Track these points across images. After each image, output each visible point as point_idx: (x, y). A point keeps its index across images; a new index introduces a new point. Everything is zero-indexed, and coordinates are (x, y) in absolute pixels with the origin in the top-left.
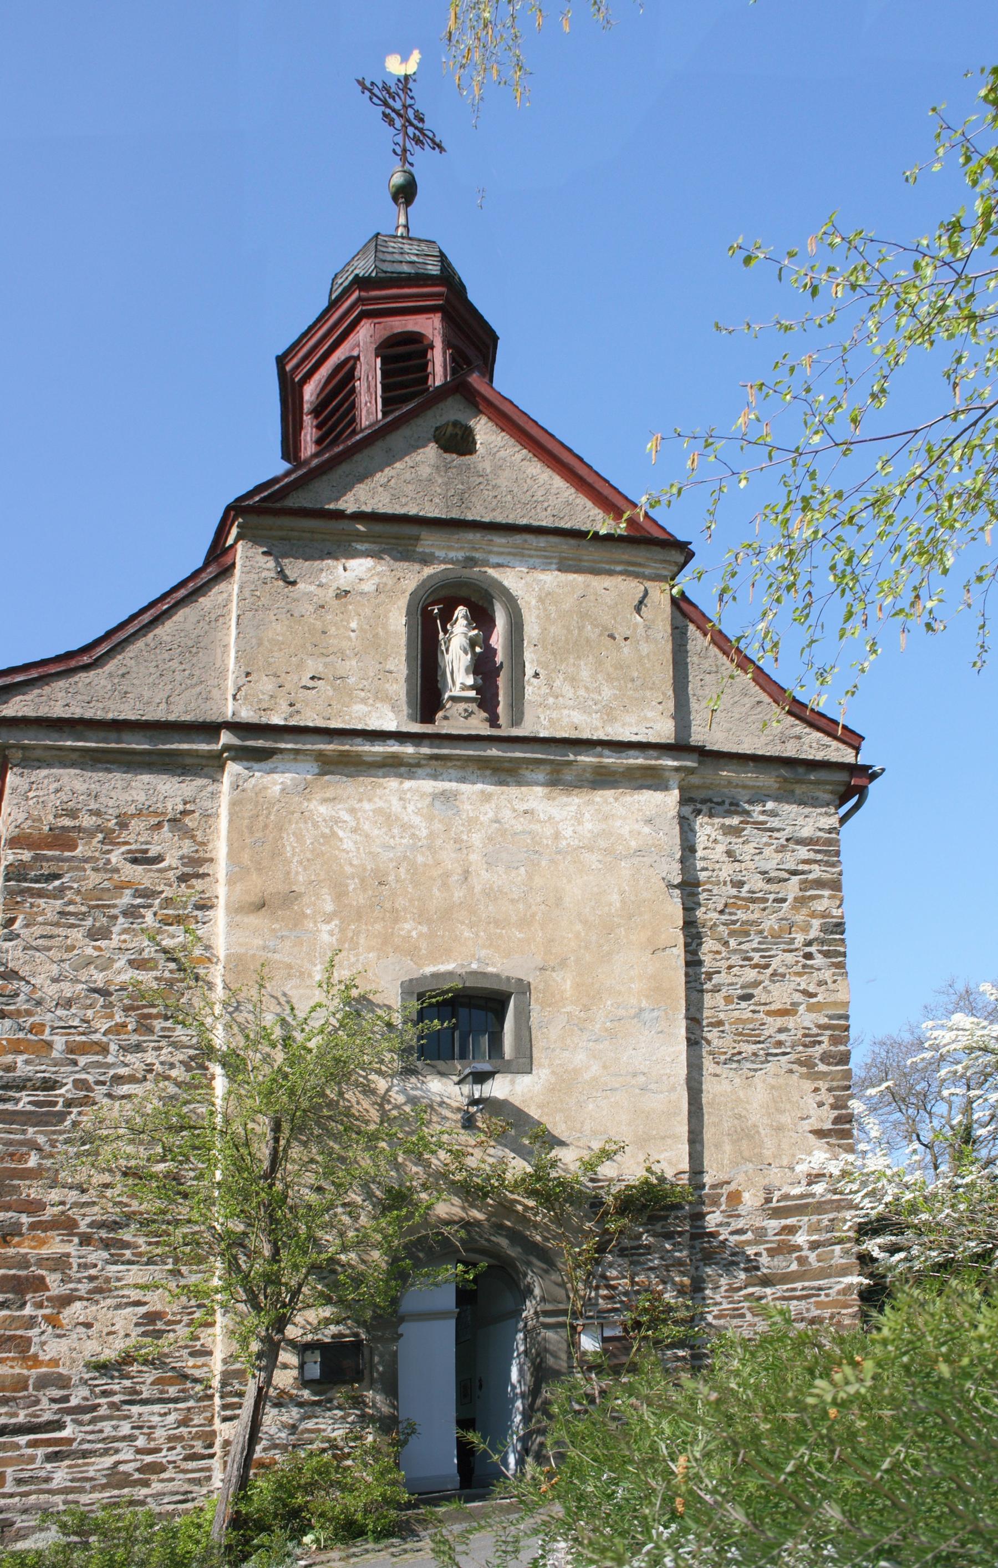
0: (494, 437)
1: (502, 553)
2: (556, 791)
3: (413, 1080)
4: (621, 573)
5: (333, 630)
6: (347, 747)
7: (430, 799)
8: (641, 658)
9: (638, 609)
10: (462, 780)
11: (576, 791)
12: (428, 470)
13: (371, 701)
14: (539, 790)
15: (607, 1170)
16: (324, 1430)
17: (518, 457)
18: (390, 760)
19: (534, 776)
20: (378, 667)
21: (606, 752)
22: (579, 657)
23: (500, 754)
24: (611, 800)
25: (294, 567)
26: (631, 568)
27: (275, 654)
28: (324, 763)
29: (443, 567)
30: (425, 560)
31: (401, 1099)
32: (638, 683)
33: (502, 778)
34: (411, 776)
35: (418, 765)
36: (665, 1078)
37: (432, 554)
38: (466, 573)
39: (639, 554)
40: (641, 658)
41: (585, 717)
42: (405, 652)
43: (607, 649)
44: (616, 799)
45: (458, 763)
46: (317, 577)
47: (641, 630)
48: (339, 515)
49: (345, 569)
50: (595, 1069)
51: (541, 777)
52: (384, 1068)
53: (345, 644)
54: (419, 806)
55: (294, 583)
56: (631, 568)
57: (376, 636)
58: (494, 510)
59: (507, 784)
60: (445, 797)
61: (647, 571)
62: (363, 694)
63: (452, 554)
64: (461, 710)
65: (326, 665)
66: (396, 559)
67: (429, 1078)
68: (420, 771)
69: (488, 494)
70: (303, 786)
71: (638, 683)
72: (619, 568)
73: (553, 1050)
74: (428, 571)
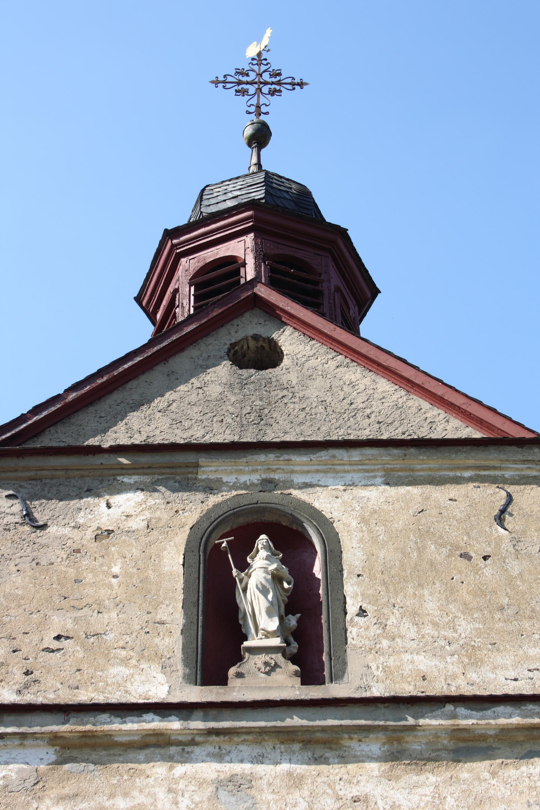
0: (301, 347)
1: (308, 472)
2: (400, 768)
4: (471, 479)
5: (89, 578)
6: (89, 727)
7: (212, 788)
8: (510, 581)
9: (500, 519)
10: (260, 759)
11: (430, 766)
12: (219, 389)
13: (134, 662)
14: (374, 768)
17: (332, 364)
18: (153, 740)
19: (364, 747)
20: (146, 617)
21: (461, 710)
22: (421, 585)
23: (305, 722)
24: (486, 775)
25: (43, 510)
26: (483, 473)
27: (12, 612)
28: (63, 747)
29: (234, 493)
30: (210, 488)
32: (510, 612)
33: (318, 753)
34: (185, 758)
35: (193, 743)
37: (219, 480)
38: (265, 497)
39: (492, 457)
40: (510, 581)
41: (435, 662)
42: (182, 597)
43: (460, 572)
44: (494, 774)
45: (250, 737)
46: (73, 518)
47: (507, 545)
48: (97, 450)
49: (109, 506)
51: (374, 746)
53: (103, 593)
54: (197, 799)
55: (44, 527)
56: (483, 473)
57: (145, 580)
58: (301, 423)
59: (326, 762)
60: (235, 784)
61: (508, 474)
62: (123, 653)
63: (243, 478)
64: (260, 664)
65: (76, 620)
66: (174, 490)
68: (197, 750)
69: (294, 407)
70: (33, 780)
71: (510, 612)
72: (467, 474)
74: (214, 500)
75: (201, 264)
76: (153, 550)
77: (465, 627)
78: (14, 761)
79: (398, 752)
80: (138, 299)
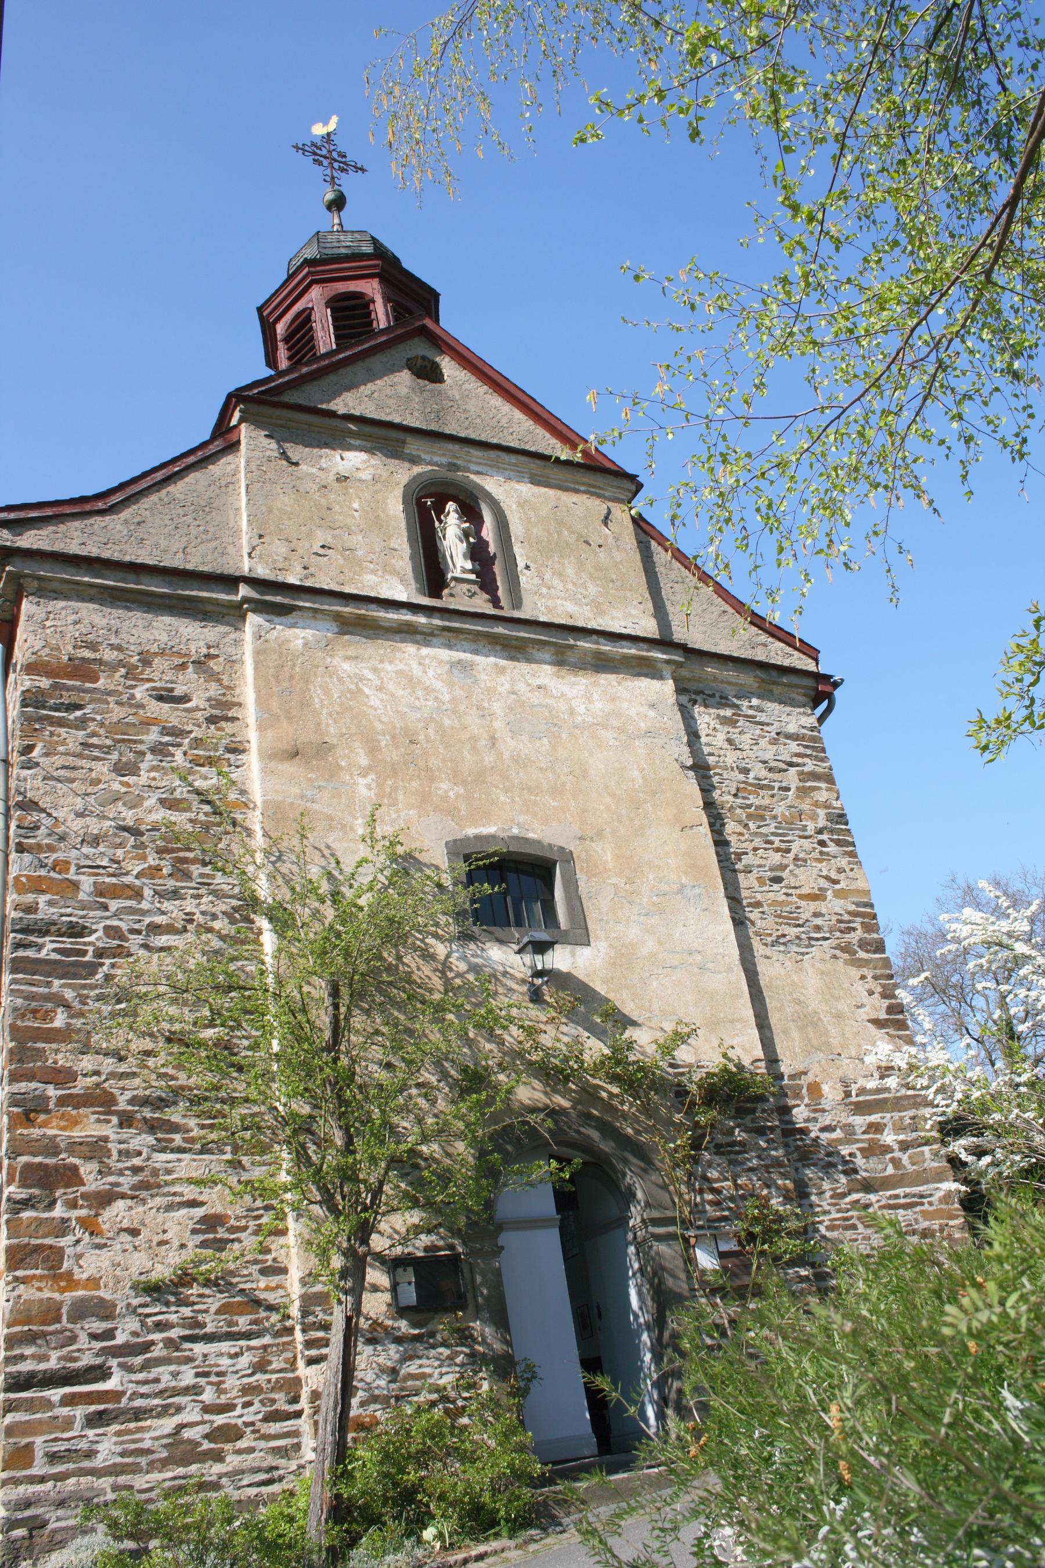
2: (564, 671)
3: (472, 946)
4: (584, 492)
5: (337, 508)
6: (363, 612)
11: (581, 673)
15: (684, 1054)
16: (430, 1376)
18: (405, 628)
21: (601, 640)
23: (506, 632)
24: (615, 683)
25: (295, 452)
29: (430, 468)
30: (414, 460)
31: (462, 967)
32: (618, 584)
34: (428, 645)
35: (432, 634)
36: (720, 957)
37: (419, 457)
38: (451, 475)
41: (577, 608)
44: (619, 683)
47: (611, 541)
48: (332, 414)
50: (650, 945)
52: (440, 932)
61: (607, 494)
63: (436, 459)
65: (334, 537)
66: (387, 456)
67: (488, 945)
68: (434, 640)
72: (582, 488)
73: (607, 922)
74: (417, 470)
75: (334, 293)
76: (379, 496)
77: (593, 589)
78: (309, 627)
79: (561, 660)
80: (260, 310)
